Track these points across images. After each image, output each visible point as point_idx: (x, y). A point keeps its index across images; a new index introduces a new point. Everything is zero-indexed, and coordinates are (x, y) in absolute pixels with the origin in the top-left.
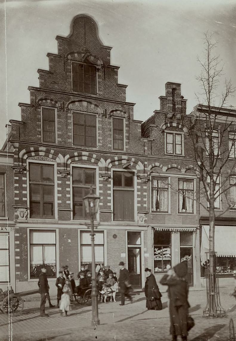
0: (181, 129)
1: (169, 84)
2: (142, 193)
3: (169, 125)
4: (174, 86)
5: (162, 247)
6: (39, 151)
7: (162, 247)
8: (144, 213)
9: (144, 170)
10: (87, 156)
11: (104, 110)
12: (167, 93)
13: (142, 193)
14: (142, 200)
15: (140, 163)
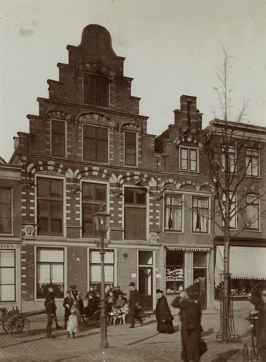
0: (196, 145)
3: (183, 140)
4: (190, 100)
8: (156, 232)
9: (157, 186)
10: (98, 171)
13: (155, 211)
14: (154, 217)
15: (152, 179)
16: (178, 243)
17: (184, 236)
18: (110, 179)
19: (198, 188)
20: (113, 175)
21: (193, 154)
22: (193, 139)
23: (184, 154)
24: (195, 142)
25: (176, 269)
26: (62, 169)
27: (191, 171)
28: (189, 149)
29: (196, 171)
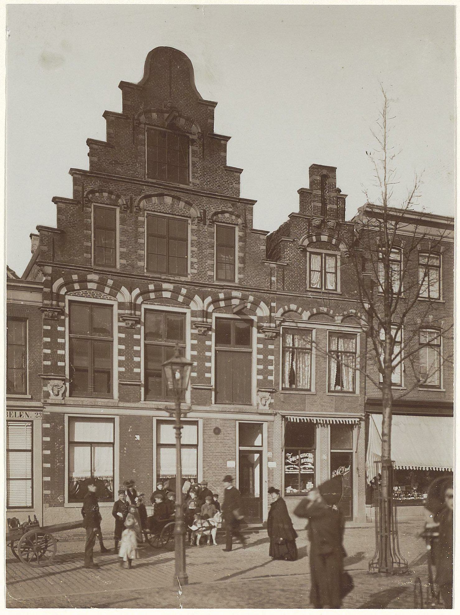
2: (265, 357)
4: (325, 172)
8: (269, 392)
10: (171, 291)
12: (312, 183)
13: (265, 357)
14: (266, 368)
15: (262, 304)
17: (315, 397)
18: (192, 305)
19: (339, 319)
20: (197, 298)
22: (331, 237)
23: (316, 263)
24: (334, 241)
25: (301, 453)
27: (326, 291)
28: (323, 255)
29: (336, 290)
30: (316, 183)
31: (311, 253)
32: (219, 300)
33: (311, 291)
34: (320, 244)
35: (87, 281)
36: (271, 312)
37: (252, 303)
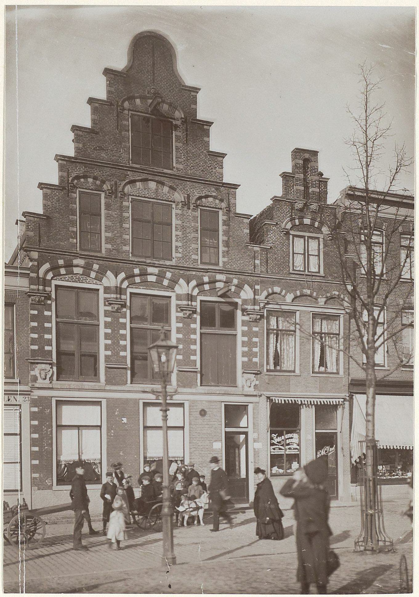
0: (319, 230)
1: (297, 152)
4: (307, 156)
5: (285, 432)
6: (72, 266)
7: (285, 432)
8: (254, 374)
9: (254, 299)
10: (156, 275)
11: (186, 196)
12: (295, 166)
13: (250, 339)
15: (246, 287)
16: (289, 391)
20: (181, 281)
21: (313, 245)
22: (313, 220)
23: (299, 245)
24: (316, 224)
26: (97, 272)
27: (309, 274)
28: (306, 238)
29: (319, 272)
30: (299, 167)
31: (294, 236)
32: (134, 276)
33: (294, 274)
34: (302, 227)
35: (72, 266)
36: (255, 295)
37: (236, 286)
